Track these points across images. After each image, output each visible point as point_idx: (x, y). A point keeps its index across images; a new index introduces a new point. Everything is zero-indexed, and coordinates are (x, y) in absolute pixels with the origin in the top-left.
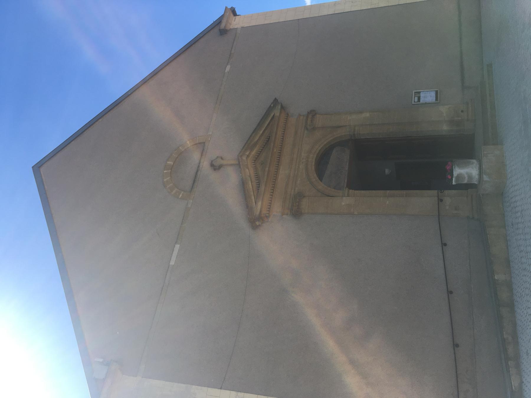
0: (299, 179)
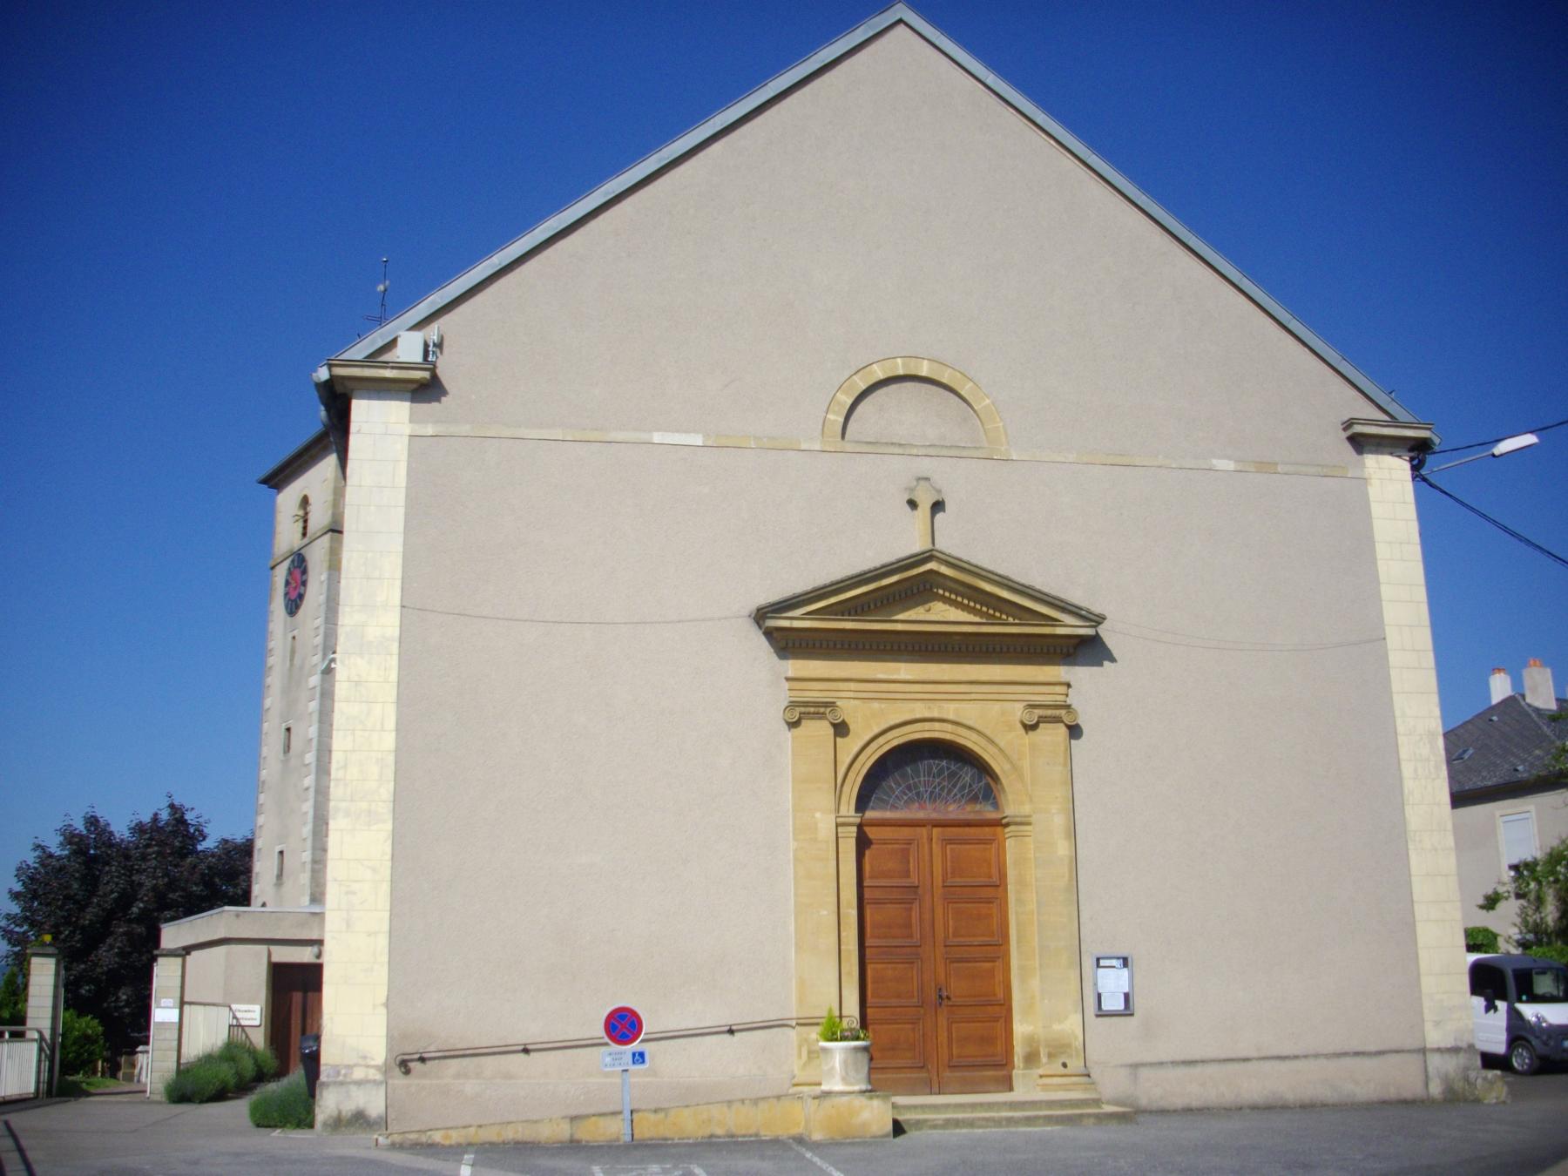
0: (883, 706)
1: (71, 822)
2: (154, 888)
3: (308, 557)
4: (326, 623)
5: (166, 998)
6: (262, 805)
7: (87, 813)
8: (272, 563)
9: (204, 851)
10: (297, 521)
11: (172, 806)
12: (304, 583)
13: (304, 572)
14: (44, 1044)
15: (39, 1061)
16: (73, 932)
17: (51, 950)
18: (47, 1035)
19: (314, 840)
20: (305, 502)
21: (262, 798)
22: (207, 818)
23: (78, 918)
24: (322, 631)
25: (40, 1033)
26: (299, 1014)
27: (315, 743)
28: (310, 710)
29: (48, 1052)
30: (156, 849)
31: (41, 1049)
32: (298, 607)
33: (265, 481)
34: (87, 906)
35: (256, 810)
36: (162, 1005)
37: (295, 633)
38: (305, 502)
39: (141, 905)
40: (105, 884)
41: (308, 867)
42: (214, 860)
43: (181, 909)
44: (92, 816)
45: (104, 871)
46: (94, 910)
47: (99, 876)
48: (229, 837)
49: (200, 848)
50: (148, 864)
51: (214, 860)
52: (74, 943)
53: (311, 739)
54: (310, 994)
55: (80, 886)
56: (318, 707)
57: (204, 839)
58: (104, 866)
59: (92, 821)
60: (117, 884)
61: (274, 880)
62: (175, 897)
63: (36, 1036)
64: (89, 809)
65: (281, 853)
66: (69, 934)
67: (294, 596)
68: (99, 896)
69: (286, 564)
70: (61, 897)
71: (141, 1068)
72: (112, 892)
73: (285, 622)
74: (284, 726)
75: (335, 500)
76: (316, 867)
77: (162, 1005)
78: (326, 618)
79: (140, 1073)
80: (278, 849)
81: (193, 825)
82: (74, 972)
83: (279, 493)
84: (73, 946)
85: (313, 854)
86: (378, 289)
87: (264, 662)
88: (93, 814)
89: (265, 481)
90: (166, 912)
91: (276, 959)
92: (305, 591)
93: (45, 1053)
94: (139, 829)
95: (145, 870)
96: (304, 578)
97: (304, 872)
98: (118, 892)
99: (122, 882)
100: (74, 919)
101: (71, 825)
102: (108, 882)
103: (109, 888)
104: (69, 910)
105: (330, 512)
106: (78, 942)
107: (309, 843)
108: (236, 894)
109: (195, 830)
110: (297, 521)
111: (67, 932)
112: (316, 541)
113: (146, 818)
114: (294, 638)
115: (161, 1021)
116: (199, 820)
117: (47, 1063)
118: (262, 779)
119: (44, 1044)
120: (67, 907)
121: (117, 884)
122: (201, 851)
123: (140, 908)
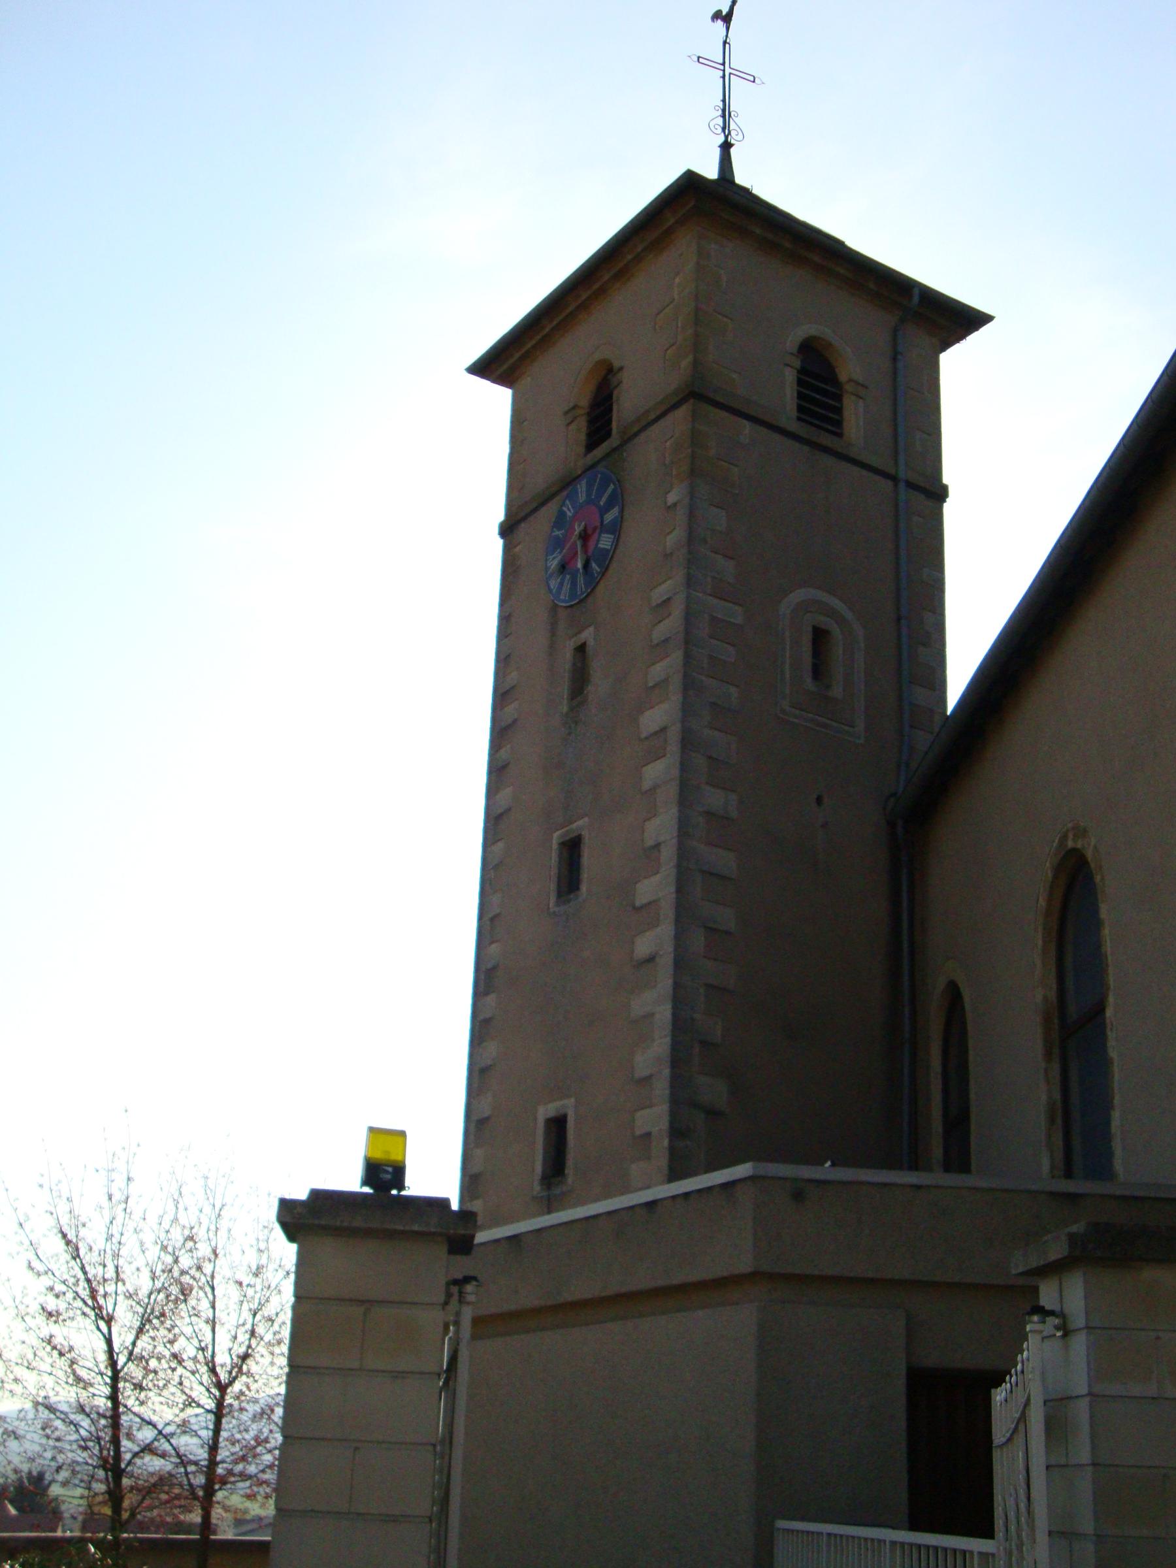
27: (668, 854)
37: (588, 635)
53: (657, 846)
56: (676, 772)
92: (616, 543)
105: (686, 363)
107: (661, 1087)
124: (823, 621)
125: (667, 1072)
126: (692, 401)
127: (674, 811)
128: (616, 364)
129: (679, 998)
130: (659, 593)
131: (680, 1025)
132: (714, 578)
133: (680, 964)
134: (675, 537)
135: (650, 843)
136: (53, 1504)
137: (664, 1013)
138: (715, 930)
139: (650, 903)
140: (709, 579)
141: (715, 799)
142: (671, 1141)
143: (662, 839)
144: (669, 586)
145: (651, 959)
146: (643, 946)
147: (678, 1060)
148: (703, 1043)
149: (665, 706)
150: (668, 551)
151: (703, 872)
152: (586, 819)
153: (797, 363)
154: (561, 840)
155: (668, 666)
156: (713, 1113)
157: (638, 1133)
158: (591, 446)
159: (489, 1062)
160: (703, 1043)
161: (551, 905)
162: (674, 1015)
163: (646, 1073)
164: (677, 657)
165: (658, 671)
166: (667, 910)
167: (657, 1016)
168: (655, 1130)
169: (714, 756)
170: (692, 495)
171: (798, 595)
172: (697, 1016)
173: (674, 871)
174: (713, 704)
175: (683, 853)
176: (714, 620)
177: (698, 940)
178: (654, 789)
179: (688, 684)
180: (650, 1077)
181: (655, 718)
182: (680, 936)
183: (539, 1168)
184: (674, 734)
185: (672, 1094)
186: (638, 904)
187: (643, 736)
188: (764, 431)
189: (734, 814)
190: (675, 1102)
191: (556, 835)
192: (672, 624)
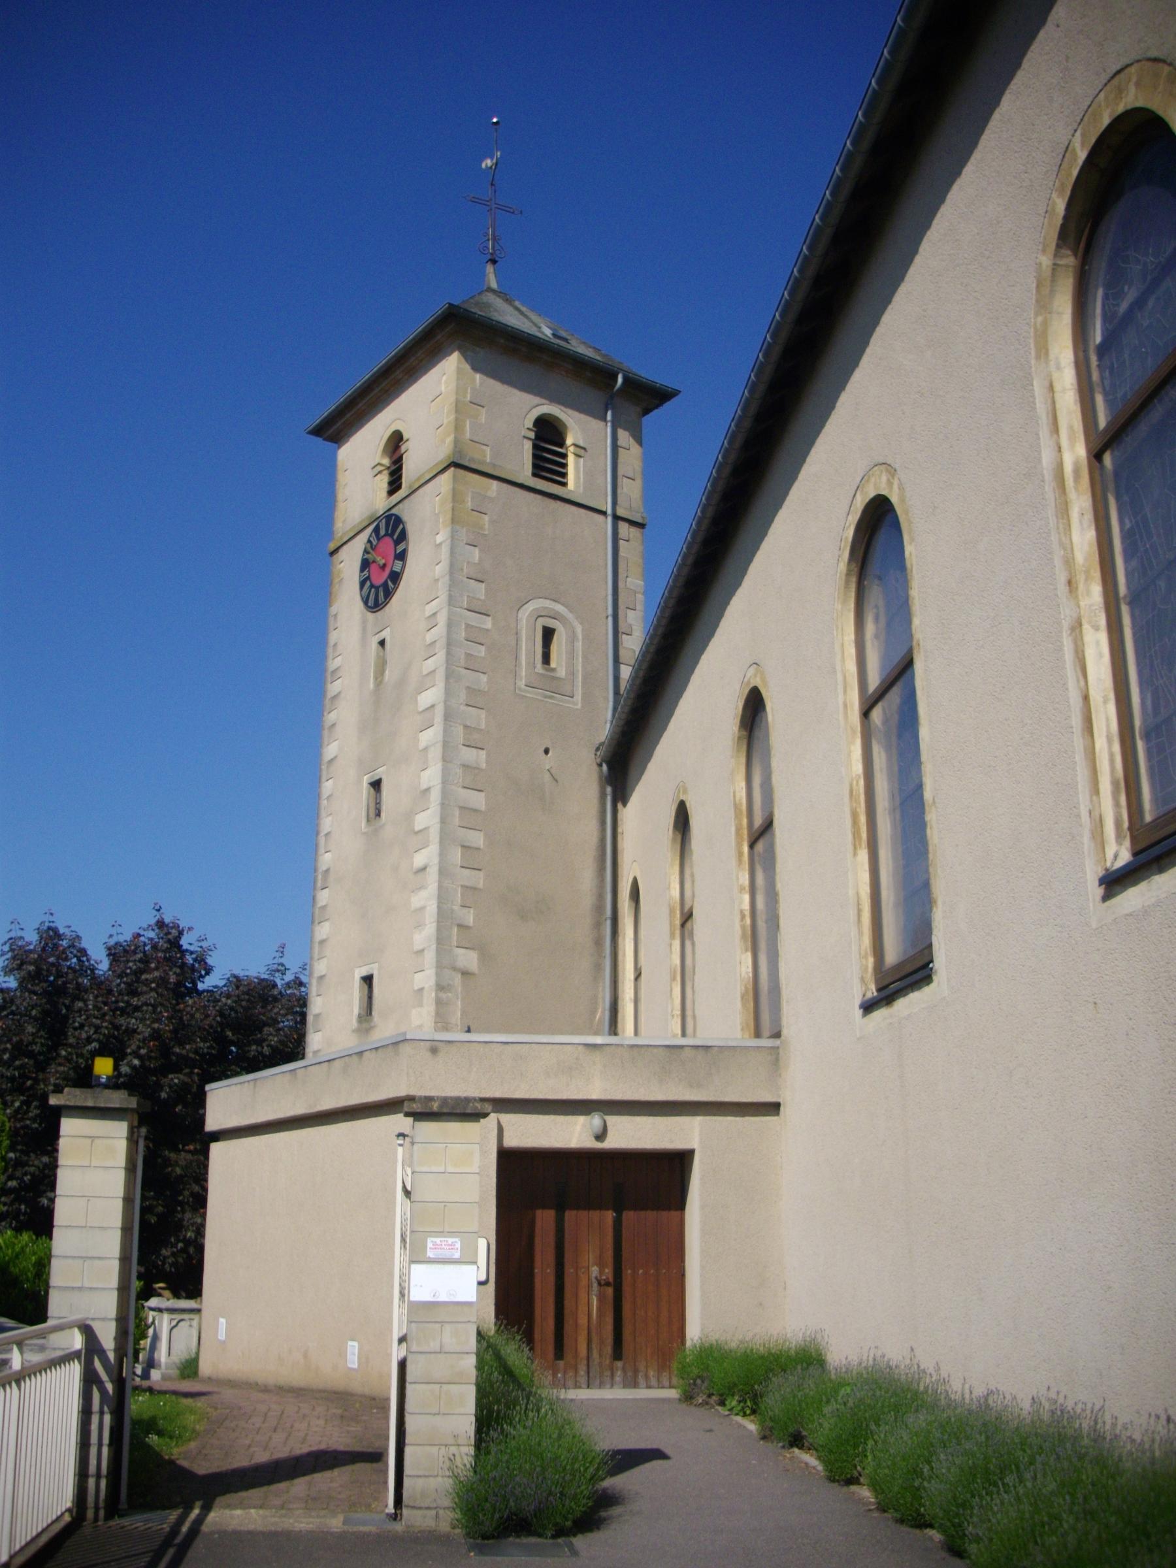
1: (20, 933)
2: (156, 1035)
3: (405, 518)
4: (449, 605)
5: (440, 1233)
6: (324, 907)
7: (43, 923)
8: (332, 546)
9: (208, 991)
10: (380, 472)
11: (161, 924)
12: (402, 556)
13: (403, 537)
14: (97, 1364)
15: (86, 1412)
16: (27, 1103)
17: (117, 1099)
18: (107, 1337)
19: (439, 952)
20: (396, 442)
21: (323, 897)
22: (211, 944)
23: (36, 1081)
24: (442, 619)
25: (87, 1331)
26: (550, 1257)
27: (435, 796)
28: (422, 744)
29: (110, 1387)
30: (156, 974)
31: (90, 1379)
32: (389, 594)
33: (318, 431)
34: (48, 1062)
35: (310, 916)
36: (430, 1254)
37: (385, 634)
38: (396, 442)
39: (136, 1062)
40: (75, 1029)
41: (430, 997)
42: (229, 1002)
43: (196, 1071)
44: (49, 928)
45: (76, 1008)
46: (61, 1069)
47: (66, 1017)
48: (241, 974)
49: (200, 986)
50: (143, 999)
51: (229, 1002)
52: (28, 1122)
53: (428, 790)
54: (570, 1215)
55: (39, 1031)
56: (440, 737)
57: (208, 973)
58: (73, 1002)
59: (51, 935)
60: (97, 1028)
61: (354, 1023)
62: (184, 1052)
63: (77, 1341)
64: (47, 918)
65: (368, 980)
66: (19, 1108)
67: (380, 578)
68: (71, 1046)
69: (360, 543)
70: (9, 1046)
71: (156, 1338)
72: (89, 1040)
73: (364, 622)
74: (366, 780)
75: (457, 419)
76: (443, 995)
77: (430, 1254)
78: (450, 597)
79: (153, 1347)
80: (364, 972)
81: (192, 953)
82: (32, 1169)
83: (339, 447)
84: (27, 1127)
85: (437, 975)
86: (483, 166)
87: (321, 691)
88: (51, 924)
89: (318, 431)
90: (170, 1076)
91: (511, 1142)
92: (403, 567)
93: (103, 1391)
94: (116, 954)
95: (137, 1008)
96: (400, 548)
97: (421, 1005)
98: (98, 1040)
99: (105, 1024)
100: (29, 1083)
101: (22, 938)
102: (82, 1026)
103: (84, 1035)
104: (22, 1066)
105: (450, 439)
106: (34, 1120)
107: (430, 957)
108: (261, 1053)
109: (195, 960)
110: (380, 472)
111: (17, 1104)
112: (421, 491)
113: (126, 936)
114: (382, 643)
115: (427, 1297)
116: (204, 944)
117: (107, 1418)
118: (322, 867)
119: (97, 1364)
120: (17, 1063)
121: (97, 1028)
122: (204, 991)
123: (134, 1068)
124: (551, 623)
125: (434, 947)
126: (452, 469)
127: (439, 766)
128: (405, 437)
129: (442, 897)
130: (430, 609)
131: (443, 915)
132: (468, 596)
133: (443, 872)
134: (441, 569)
135: (424, 786)
136: (703, 1354)
137: (432, 908)
138: (469, 847)
139: (425, 829)
140: (465, 598)
141: (470, 755)
142: (436, 994)
143: (431, 784)
144: (439, 605)
145: (424, 869)
146: (419, 860)
147: (441, 940)
148: (460, 926)
149: (433, 690)
150: (437, 578)
151: (461, 808)
152: (385, 767)
153: (532, 435)
154: (370, 781)
155: (437, 662)
156: (465, 974)
157: (416, 988)
158: (391, 493)
159: (324, 937)
160: (460, 926)
161: (363, 827)
162: (439, 907)
163: (421, 948)
164: (441, 656)
165: (430, 664)
166: (434, 835)
167: (428, 908)
168: (426, 986)
169: (469, 724)
170: (452, 537)
171: (531, 607)
172: (456, 908)
173: (438, 808)
174: (468, 688)
175: (445, 794)
176: (467, 626)
177: (456, 855)
178: (426, 749)
179: (449, 676)
180: (423, 950)
181: (428, 697)
182: (442, 854)
183: (356, 1011)
184: (439, 712)
185: (437, 961)
186: (417, 829)
187: (421, 709)
188: (505, 486)
189: (484, 766)
190: (440, 966)
191: (366, 777)
192: (440, 631)
